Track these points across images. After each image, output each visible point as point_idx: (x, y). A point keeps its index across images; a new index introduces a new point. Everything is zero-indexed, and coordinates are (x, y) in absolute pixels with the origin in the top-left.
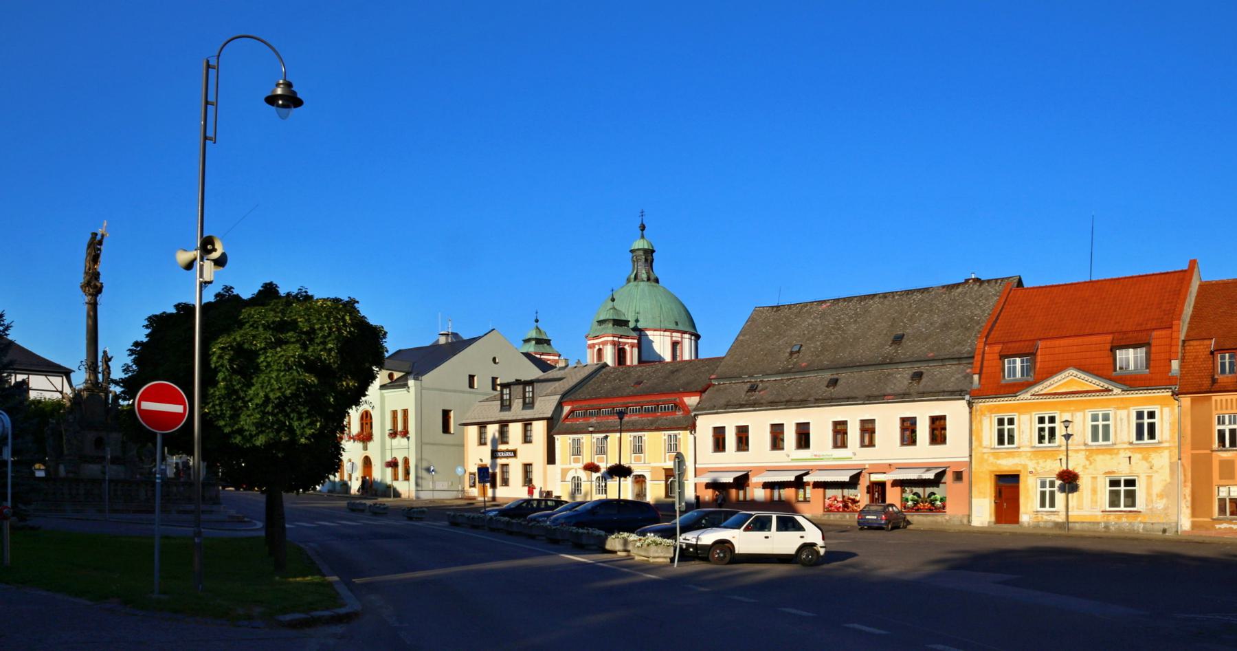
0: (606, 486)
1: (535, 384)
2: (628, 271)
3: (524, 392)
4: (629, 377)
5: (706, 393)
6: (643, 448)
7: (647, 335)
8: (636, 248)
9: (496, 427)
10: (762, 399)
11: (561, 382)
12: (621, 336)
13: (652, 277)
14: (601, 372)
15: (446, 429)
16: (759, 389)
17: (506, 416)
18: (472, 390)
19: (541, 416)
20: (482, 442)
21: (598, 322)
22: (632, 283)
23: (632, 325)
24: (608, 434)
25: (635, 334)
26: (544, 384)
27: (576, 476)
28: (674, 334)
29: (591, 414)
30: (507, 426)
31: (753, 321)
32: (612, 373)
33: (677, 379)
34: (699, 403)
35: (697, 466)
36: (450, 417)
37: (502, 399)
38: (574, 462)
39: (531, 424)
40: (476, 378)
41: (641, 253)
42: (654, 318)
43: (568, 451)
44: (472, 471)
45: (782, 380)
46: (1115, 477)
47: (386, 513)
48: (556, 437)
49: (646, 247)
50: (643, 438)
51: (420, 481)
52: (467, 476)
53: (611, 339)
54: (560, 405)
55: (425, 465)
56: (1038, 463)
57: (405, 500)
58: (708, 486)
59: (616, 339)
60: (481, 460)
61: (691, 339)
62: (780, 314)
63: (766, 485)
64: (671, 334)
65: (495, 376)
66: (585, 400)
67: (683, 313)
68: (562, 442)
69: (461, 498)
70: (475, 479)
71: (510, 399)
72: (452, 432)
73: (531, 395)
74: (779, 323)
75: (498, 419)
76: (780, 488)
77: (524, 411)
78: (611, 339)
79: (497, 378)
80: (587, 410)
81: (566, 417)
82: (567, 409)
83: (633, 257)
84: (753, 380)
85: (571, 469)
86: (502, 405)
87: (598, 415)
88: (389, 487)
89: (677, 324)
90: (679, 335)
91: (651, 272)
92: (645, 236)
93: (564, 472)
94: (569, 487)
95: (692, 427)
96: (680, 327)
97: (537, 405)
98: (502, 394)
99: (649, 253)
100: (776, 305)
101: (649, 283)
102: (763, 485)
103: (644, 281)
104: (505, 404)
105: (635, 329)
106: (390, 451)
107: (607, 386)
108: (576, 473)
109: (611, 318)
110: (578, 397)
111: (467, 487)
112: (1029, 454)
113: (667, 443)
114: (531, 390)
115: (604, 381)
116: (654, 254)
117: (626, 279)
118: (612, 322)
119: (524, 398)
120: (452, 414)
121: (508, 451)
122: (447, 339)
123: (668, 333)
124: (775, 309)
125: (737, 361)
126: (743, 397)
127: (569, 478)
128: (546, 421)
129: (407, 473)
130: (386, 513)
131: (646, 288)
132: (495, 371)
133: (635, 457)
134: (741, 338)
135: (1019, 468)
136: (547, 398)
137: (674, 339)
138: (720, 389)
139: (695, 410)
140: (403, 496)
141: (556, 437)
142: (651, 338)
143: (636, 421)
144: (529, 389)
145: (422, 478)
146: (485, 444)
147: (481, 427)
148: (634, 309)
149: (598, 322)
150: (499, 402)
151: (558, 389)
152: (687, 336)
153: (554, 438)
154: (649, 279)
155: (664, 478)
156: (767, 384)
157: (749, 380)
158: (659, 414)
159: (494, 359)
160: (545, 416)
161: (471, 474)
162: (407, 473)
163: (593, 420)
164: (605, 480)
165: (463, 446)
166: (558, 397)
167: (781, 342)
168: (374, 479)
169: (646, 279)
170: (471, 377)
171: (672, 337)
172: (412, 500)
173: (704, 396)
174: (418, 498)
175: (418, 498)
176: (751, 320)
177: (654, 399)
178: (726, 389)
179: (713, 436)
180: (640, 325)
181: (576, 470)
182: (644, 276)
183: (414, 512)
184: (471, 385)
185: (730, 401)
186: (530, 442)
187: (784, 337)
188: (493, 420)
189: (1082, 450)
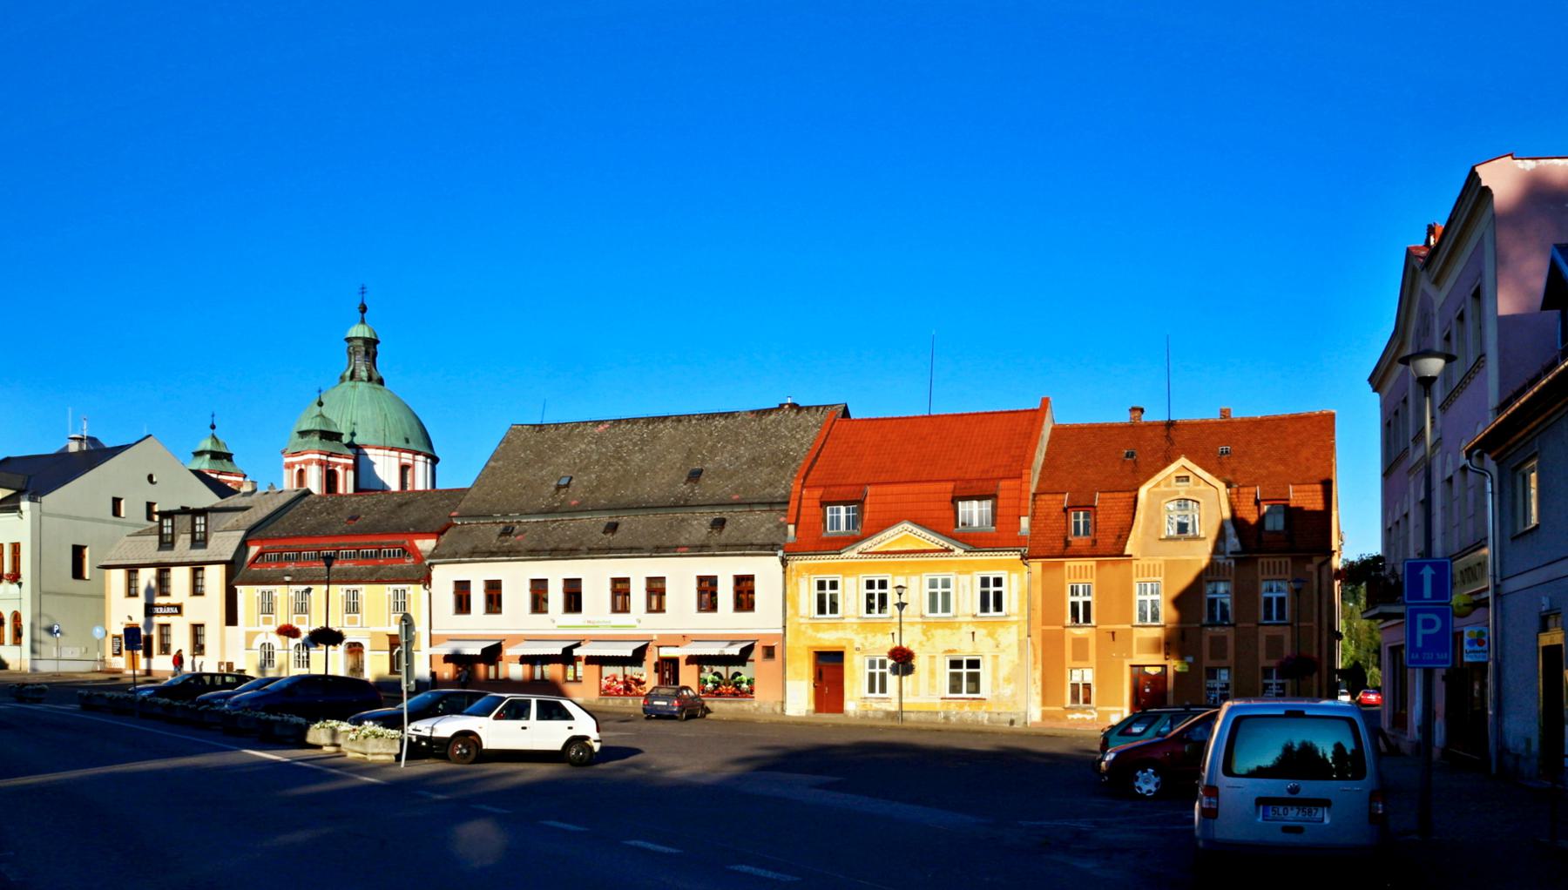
1: (209, 514)
3: (194, 525)
5: (446, 535)
7: (366, 455)
8: (354, 336)
10: (519, 545)
11: (246, 512)
12: (332, 453)
13: (375, 377)
14: (303, 502)
15: (78, 573)
16: (515, 532)
17: (166, 556)
18: (117, 519)
19: (217, 559)
20: (131, 592)
22: (348, 383)
23: (346, 439)
24: (311, 586)
25: (349, 452)
26: (221, 515)
27: (267, 642)
28: (403, 455)
30: (169, 570)
31: (508, 442)
33: (406, 515)
34: (435, 548)
35: (433, 632)
36: (84, 556)
37: (161, 534)
39: (202, 569)
40: (123, 502)
41: (360, 343)
42: (376, 431)
45: (545, 521)
46: (956, 657)
48: (239, 588)
49: (367, 335)
50: (360, 593)
53: (317, 456)
54: (244, 546)
55: (46, 623)
56: (866, 638)
57: (13, 673)
59: (324, 457)
60: (130, 618)
61: (426, 462)
63: (524, 660)
64: (400, 455)
66: (280, 538)
67: (416, 427)
68: (248, 596)
69: (100, 672)
70: (121, 644)
71: (173, 534)
72: (87, 577)
73: (203, 529)
75: (154, 561)
77: (193, 551)
81: (253, 561)
82: (254, 550)
83: (349, 348)
84: (508, 521)
85: (259, 633)
87: (297, 559)
89: (407, 441)
90: (410, 456)
91: (374, 369)
93: (250, 637)
95: (426, 580)
96: (412, 446)
97: (211, 543)
98: (161, 526)
99: (371, 344)
100: (539, 423)
101: (370, 384)
104: (165, 540)
105: (351, 445)
107: (310, 521)
108: (267, 638)
109: (318, 428)
112: (855, 627)
115: (306, 513)
116: (378, 346)
117: (338, 377)
119: (193, 533)
122: (80, 446)
123: (395, 453)
124: (537, 428)
125: (488, 495)
126: (494, 542)
127: (257, 644)
129: (18, 634)
131: (367, 391)
132: (151, 493)
134: (492, 464)
135: (843, 644)
137: (403, 461)
139: (430, 557)
140: (11, 667)
141: (239, 588)
142: (372, 458)
144: (200, 520)
145: (40, 642)
146: (136, 595)
151: (242, 523)
152: (421, 458)
153: (236, 590)
154: (370, 379)
155: (388, 648)
157: (502, 520)
159: (150, 478)
161: (114, 637)
162: (18, 634)
163: (291, 567)
164: (308, 649)
165: (103, 597)
166: (242, 533)
167: (544, 472)
169: (366, 379)
170: (116, 502)
172: (25, 673)
173: (443, 539)
174: (34, 670)
175: (34, 670)
176: (506, 441)
180: (357, 440)
181: (267, 633)
182: (364, 374)
184: (116, 512)
185: (476, 547)
186: (202, 594)
188: (147, 562)
189: (918, 623)
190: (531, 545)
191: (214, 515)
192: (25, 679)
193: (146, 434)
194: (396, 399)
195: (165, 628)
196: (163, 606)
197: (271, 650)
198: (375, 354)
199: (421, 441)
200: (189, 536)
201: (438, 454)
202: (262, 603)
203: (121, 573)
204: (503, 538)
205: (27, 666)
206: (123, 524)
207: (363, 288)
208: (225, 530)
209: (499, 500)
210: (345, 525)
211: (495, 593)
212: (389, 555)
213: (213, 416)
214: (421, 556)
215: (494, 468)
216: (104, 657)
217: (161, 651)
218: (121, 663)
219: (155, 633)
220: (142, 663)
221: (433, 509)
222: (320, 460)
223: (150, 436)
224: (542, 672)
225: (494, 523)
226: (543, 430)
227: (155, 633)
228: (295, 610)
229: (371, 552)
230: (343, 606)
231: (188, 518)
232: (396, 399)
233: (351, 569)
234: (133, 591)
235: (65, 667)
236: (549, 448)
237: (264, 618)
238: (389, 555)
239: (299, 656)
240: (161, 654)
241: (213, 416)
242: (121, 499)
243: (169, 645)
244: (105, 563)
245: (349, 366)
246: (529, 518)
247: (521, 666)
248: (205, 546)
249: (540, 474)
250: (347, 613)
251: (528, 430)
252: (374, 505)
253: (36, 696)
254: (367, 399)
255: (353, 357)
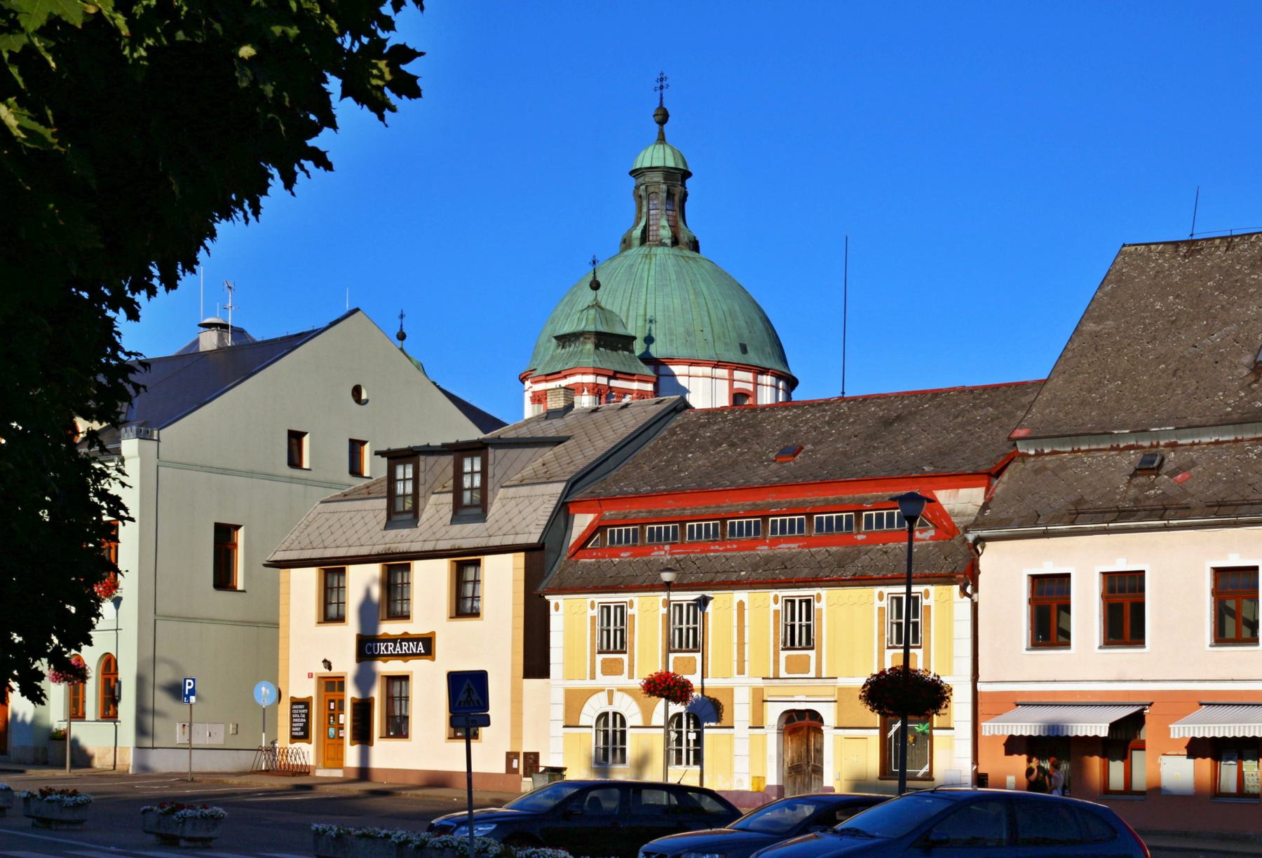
0: (699, 741)
1: (490, 450)
2: (624, 217)
3: (459, 474)
4: (758, 435)
5: (1005, 477)
6: (814, 635)
7: (673, 375)
8: (647, 164)
9: (375, 569)
10: (1186, 493)
11: (559, 449)
12: (616, 372)
13: (683, 237)
14: (673, 424)
15: (223, 578)
16: (1168, 466)
17: (403, 540)
19: (508, 541)
20: (330, 614)
21: (557, 338)
22: (636, 251)
23: (639, 348)
24: (708, 593)
25: (648, 371)
26: (513, 453)
27: (610, 709)
28: (738, 374)
29: (656, 537)
30: (407, 568)
31: (1119, 281)
32: (703, 426)
33: (905, 441)
34: (985, 507)
36: (235, 545)
37: (391, 495)
38: (604, 673)
39: (477, 564)
40: (306, 440)
41: (658, 177)
42: (688, 333)
43: (586, 637)
44: (301, 695)
45: (1236, 441)
47: (80, 822)
48: (553, 599)
49: (670, 163)
50: (816, 605)
51: (149, 720)
52: (285, 709)
53: (590, 379)
54: (563, 511)
55: (165, 675)
57: (102, 776)
58: (1014, 745)
59: (603, 381)
60: (328, 665)
61: (777, 388)
62: (1202, 262)
63: (1196, 748)
64: (731, 375)
65: (358, 436)
66: (638, 496)
67: (759, 325)
69: (267, 771)
70: (308, 716)
71: (416, 495)
72: (240, 587)
73: (477, 483)
74: (1204, 285)
75: (378, 549)
76: (1241, 757)
77: (457, 527)
78: (590, 379)
79: (364, 443)
80: (643, 525)
81: (582, 544)
82: (582, 522)
83: (637, 188)
84: (1146, 443)
86: (391, 510)
87: (674, 540)
88: (60, 738)
89: (744, 349)
90: (749, 376)
91: (681, 223)
92: (667, 139)
93: (575, 701)
94: (589, 740)
95: (968, 577)
96: (753, 358)
97: (494, 509)
98: (392, 479)
99: (677, 177)
100: (1186, 237)
101: (675, 251)
102: (1006, 745)
103: (664, 245)
104: (399, 508)
105: (647, 359)
106: (687, 373)
107: (696, 461)
108: (611, 703)
109: (591, 328)
110: (615, 489)
111: (283, 741)
113: (887, 620)
114: (477, 467)
115: (685, 446)
116: (688, 182)
117: (620, 240)
118: (593, 339)
119: (458, 490)
120: (240, 536)
121: (406, 638)
122: (221, 338)
123: (723, 372)
124: (1183, 249)
125: (1090, 391)
126: (1123, 489)
127: (589, 715)
128: (522, 555)
129: (111, 698)
130: (80, 822)
131: (671, 262)
132: (357, 422)
133: (788, 658)
134: (1090, 326)
136: (524, 491)
137: (737, 385)
138: (1044, 468)
139: (976, 525)
140: (97, 763)
141: (553, 599)
142: (682, 381)
143: (793, 557)
144: (471, 464)
145: (154, 712)
146: (340, 619)
147: (327, 571)
148: (641, 312)
149: (557, 338)
150: (383, 503)
151: (555, 468)
152: (767, 379)
153: (548, 603)
154: (675, 242)
156: (1194, 455)
157: (1132, 442)
158: (860, 537)
159: (357, 391)
160: (521, 540)
161: (295, 702)
162: (111, 698)
163: (662, 554)
164: (698, 725)
165: (275, 625)
166: (559, 488)
167: (1217, 338)
168: (15, 716)
169: (668, 242)
170: (295, 438)
171: (732, 381)
172: (123, 776)
173: (1000, 485)
174: (142, 767)
175: (142, 767)
176: (1115, 279)
177: (848, 496)
178: (1063, 467)
179: (1030, 601)
180: (657, 351)
181: (611, 693)
182: (666, 233)
183: (184, 819)
185: (1081, 501)
186: (475, 614)
187: (1225, 324)
188: (364, 551)
190: (1218, 491)
191: (500, 453)
192: (132, 787)
193: (348, 307)
194: (721, 275)
195: (397, 685)
196: (394, 640)
197: (618, 728)
198: (684, 196)
199: (768, 349)
200: (449, 498)
201: (795, 371)
202: (602, 631)
203: (311, 576)
204: (1141, 480)
205: (128, 759)
206: (306, 482)
207: (661, 80)
208: (521, 484)
209: (1118, 401)
210: (774, 466)
211: (1127, 600)
212: (880, 524)
213: (402, 316)
214: (952, 524)
215: (1096, 335)
216: (273, 743)
217: (388, 732)
218: (307, 753)
219: (377, 694)
220: (351, 755)
221: (962, 425)
222: (596, 385)
223: (357, 310)
224: (1241, 775)
225: (1112, 449)
226: (1199, 251)
227: (377, 694)
228: (785, 643)
229: (839, 519)
230: (776, 633)
231: (447, 461)
232: (721, 275)
233: (794, 555)
234: (333, 610)
235: (206, 763)
236: (1219, 287)
237: (604, 662)
238: (880, 524)
239: (679, 741)
240: (388, 736)
241: (402, 316)
242: (304, 434)
243: (407, 718)
244: (280, 556)
245: (639, 219)
246: (1198, 435)
247: (1191, 761)
248: (482, 517)
249: (1206, 341)
250: (785, 649)
251: (1162, 253)
252: (828, 423)
253: (200, 834)
254: (674, 277)
255: (645, 203)
